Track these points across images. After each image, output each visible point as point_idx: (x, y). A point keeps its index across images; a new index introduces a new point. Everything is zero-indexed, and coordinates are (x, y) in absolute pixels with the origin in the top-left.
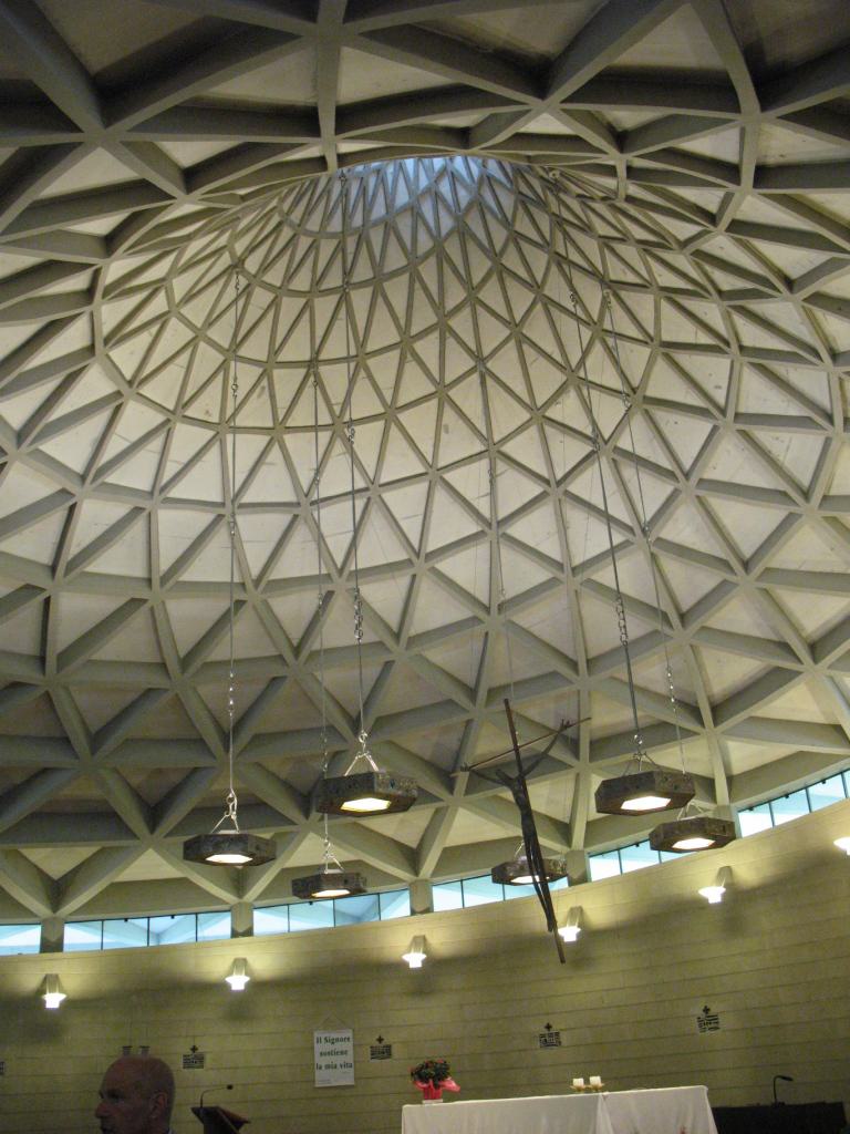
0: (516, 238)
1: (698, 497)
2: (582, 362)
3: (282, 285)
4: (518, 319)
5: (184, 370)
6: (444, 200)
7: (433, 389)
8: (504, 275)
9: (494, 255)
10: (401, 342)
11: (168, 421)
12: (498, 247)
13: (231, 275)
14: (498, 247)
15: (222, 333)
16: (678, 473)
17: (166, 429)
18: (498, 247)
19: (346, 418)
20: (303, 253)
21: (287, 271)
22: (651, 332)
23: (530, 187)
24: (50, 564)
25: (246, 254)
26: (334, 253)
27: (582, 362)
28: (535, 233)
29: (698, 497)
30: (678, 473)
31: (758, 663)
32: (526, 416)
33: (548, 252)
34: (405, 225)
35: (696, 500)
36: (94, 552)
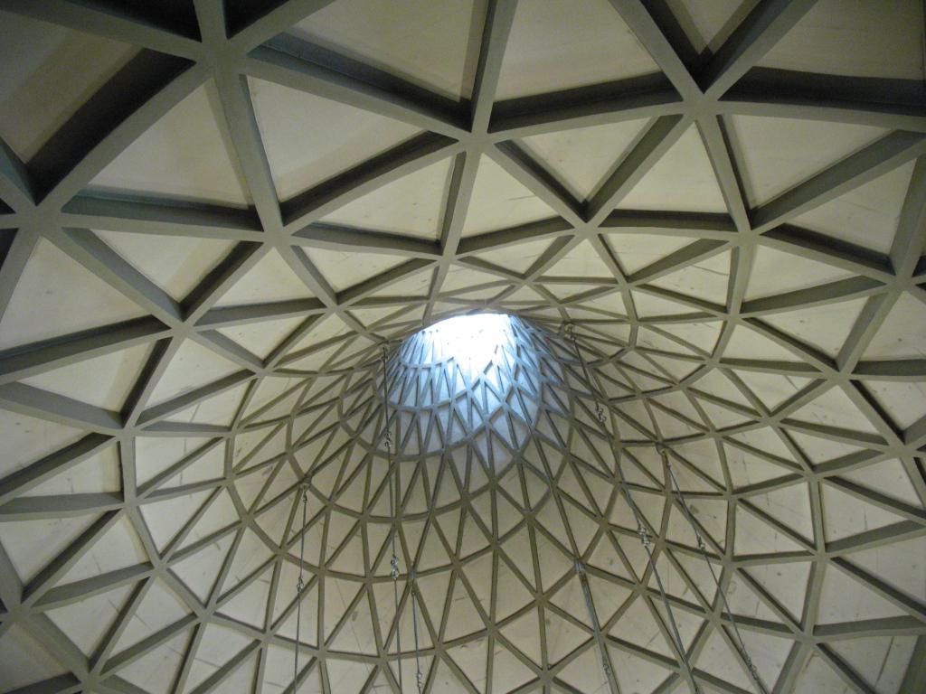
0: (575, 462)
1: (723, 626)
2: (653, 558)
3: (331, 497)
4: (640, 577)
5: (269, 586)
6: (499, 437)
7: (533, 676)
8: (616, 534)
9: (551, 480)
10: (452, 564)
11: (257, 642)
12: (554, 471)
13: (300, 490)
14: (554, 470)
15: (274, 523)
16: (706, 608)
17: (257, 649)
18: (554, 471)
19: (393, 649)
20: (351, 472)
21: (335, 486)
22: (723, 483)
23: (556, 397)
24: (89, 656)
25: (310, 473)
26: (361, 463)
27: (653, 558)
28: (649, 480)
29: (723, 626)
30: (706, 608)
31: (552, 689)
32: (529, 598)
33: (666, 494)
34: (459, 459)
35: (722, 629)
36: (40, 510)
